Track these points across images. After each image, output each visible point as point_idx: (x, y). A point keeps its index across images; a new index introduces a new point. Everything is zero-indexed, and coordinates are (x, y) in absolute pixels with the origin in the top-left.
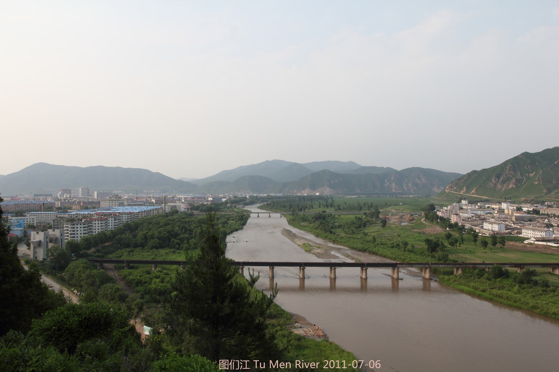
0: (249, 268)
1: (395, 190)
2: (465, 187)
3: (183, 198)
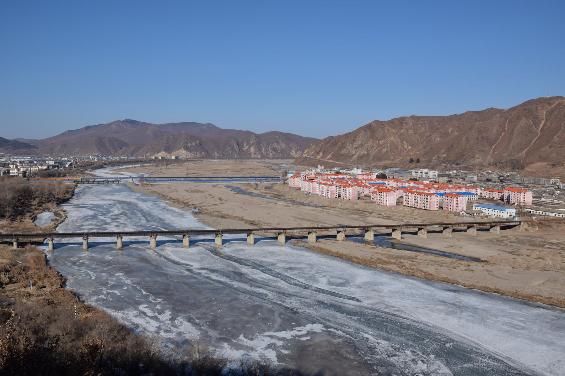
1: (255, 154)
2: (321, 152)
3: (19, 162)
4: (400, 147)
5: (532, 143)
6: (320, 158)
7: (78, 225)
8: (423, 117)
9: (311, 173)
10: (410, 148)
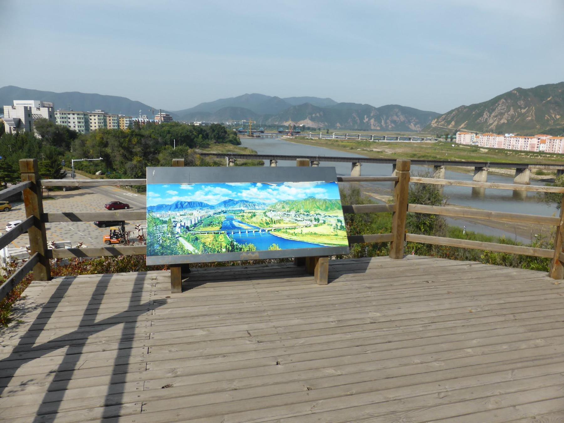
0: (9, 117)
1: (374, 126)
7: (270, 120)
10: (558, 117)
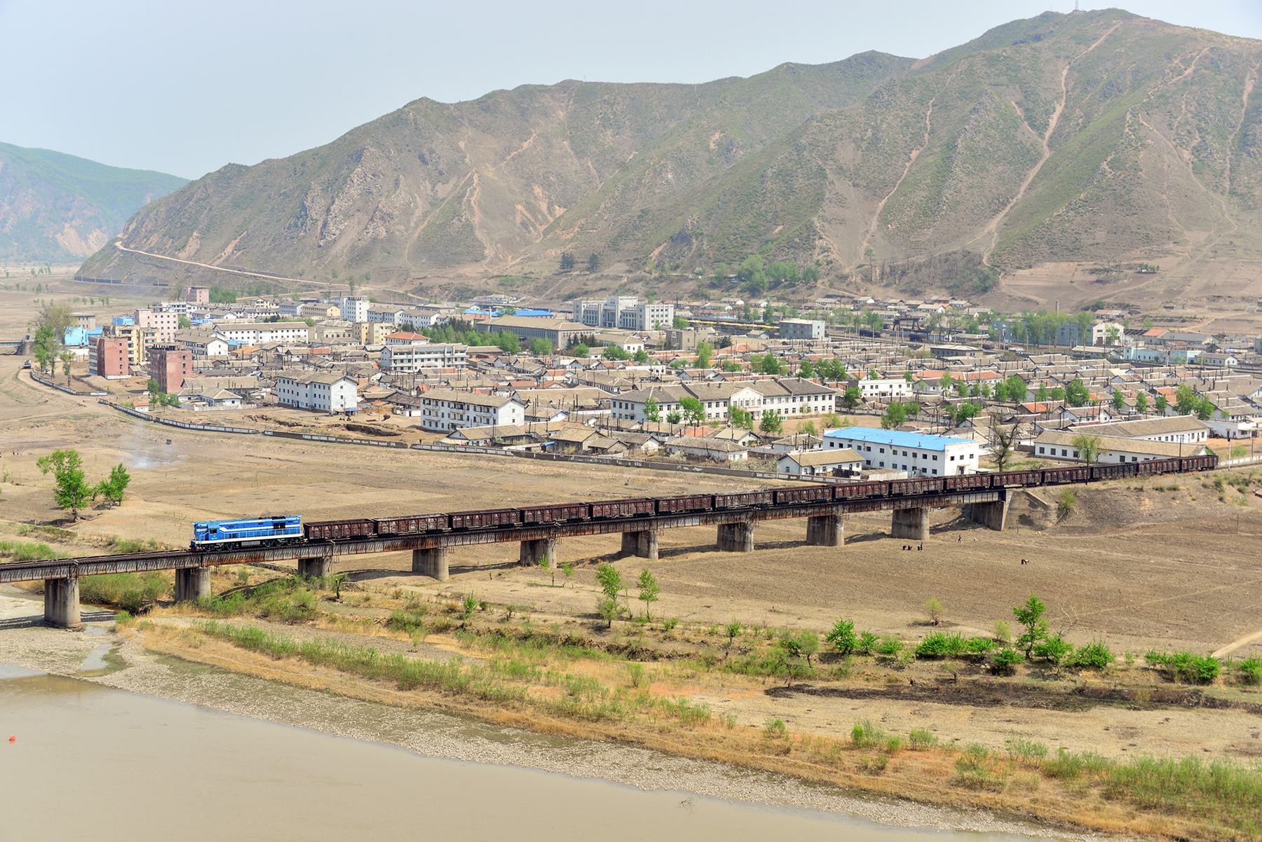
4: (519, 207)
5: (1022, 189)
6: (189, 258)
8: (608, 87)
9: (159, 319)
10: (559, 211)
